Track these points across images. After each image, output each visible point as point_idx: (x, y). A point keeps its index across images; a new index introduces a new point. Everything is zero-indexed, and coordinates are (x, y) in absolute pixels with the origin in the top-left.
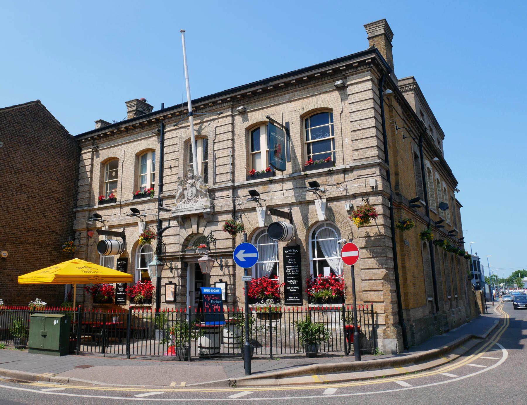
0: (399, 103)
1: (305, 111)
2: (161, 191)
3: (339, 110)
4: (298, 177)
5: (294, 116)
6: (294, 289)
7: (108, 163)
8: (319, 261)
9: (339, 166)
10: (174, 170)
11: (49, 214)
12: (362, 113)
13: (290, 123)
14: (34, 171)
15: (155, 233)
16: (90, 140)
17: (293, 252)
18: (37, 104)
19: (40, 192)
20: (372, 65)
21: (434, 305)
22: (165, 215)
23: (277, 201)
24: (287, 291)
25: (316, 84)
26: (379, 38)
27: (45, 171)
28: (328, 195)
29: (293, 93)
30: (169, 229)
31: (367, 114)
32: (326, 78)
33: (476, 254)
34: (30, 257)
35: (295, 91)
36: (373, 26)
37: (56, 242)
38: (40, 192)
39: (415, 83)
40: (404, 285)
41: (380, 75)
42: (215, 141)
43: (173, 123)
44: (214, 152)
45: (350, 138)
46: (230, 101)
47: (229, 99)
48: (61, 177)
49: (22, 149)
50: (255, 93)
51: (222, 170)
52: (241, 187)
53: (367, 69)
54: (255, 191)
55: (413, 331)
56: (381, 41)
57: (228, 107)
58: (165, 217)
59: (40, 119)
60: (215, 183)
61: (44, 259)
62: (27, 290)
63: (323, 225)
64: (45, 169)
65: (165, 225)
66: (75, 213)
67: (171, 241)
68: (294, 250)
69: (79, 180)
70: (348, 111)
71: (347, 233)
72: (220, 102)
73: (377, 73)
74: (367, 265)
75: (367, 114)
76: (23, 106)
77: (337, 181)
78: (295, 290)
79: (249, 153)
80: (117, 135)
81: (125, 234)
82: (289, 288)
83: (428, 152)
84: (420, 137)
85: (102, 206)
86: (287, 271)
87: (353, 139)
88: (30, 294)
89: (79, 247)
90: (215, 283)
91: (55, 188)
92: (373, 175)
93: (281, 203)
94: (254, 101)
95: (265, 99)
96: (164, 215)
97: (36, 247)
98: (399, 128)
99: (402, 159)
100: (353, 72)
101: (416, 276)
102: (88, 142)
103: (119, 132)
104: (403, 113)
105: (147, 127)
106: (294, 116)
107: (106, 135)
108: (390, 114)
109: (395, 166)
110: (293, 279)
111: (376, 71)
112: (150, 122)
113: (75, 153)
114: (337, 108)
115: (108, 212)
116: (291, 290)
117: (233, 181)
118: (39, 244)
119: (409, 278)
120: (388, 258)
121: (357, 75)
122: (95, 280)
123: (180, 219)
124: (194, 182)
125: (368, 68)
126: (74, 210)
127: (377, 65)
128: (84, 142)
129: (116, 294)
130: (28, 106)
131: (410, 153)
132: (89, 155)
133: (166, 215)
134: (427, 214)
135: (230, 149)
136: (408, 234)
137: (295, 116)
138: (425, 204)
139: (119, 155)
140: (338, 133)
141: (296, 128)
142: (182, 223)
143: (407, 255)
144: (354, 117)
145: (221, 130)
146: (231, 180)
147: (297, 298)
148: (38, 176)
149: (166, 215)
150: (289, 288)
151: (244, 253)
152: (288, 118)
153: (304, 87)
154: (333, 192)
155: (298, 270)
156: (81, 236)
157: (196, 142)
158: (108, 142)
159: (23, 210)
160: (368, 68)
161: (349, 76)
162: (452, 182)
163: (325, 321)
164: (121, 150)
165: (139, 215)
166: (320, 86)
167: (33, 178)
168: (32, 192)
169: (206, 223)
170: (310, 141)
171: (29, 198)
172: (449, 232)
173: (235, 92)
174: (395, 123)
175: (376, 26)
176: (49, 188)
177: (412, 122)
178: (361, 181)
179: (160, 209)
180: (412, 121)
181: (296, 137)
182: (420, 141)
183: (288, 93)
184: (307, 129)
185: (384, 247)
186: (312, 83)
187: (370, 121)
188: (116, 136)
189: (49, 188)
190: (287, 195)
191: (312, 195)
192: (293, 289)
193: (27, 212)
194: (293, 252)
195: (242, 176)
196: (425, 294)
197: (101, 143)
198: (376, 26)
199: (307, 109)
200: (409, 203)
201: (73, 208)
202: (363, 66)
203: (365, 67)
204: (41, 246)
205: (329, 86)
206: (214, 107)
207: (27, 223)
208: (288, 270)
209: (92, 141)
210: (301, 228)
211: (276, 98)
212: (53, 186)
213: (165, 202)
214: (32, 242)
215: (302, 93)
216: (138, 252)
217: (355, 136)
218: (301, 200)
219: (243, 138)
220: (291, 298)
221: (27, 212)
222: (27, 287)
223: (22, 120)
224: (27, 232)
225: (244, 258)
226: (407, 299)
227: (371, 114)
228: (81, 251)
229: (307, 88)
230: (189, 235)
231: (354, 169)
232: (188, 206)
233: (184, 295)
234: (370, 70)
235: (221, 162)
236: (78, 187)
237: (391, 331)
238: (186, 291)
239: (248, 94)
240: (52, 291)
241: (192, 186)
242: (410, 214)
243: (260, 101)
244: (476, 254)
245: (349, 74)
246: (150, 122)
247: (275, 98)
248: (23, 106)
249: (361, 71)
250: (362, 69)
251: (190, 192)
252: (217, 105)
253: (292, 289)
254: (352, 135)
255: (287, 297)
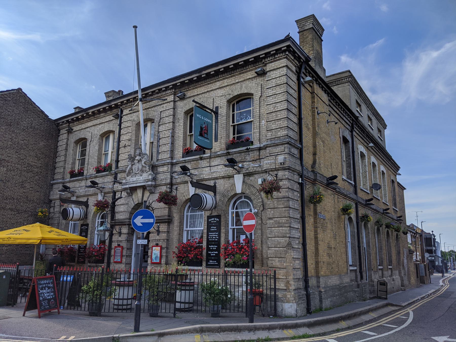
0: (325, 91)
1: (231, 96)
2: (117, 167)
3: (258, 95)
4: (222, 155)
5: (222, 101)
6: (214, 253)
7: (81, 143)
8: (236, 228)
9: (256, 145)
10: (128, 149)
11: (27, 185)
12: (276, 97)
13: (219, 108)
14: (13, 148)
15: (111, 203)
16: (66, 123)
17: (215, 220)
18: (19, 92)
19: (19, 167)
20: (287, 53)
21: (358, 273)
22: (117, 187)
23: (204, 176)
24: (208, 255)
25: (241, 72)
26: (307, 31)
27: (24, 149)
28: (245, 171)
29: (223, 81)
30: (121, 199)
31: (281, 98)
32: (250, 67)
33: (432, 232)
34: (6, 222)
35: (224, 79)
36: (303, 21)
37: (33, 210)
38: (19, 167)
39: (351, 76)
40: (316, 254)
41: (297, 63)
42: (160, 124)
43: (129, 108)
44: (158, 133)
45: (265, 120)
46: (172, 88)
47: (171, 86)
48: (40, 154)
49: (2, 129)
50: (191, 81)
51: (164, 149)
52: (176, 163)
53: (283, 57)
54: (185, 166)
55: (322, 296)
56: (310, 34)
57: (171, 93)
58: (118, 189)
59: (21, 104)
60: (158, 160)
61: (21, 223)
62: (2, 250)
63: (241, 198)
64: (25, 147)
65: (118, 195)
66: (52, 185)
67: (122, 209)
68: (216, 219)
69: (56, 157)
70: (265, 96)
71: (258, 205)
72: (164, 89)
73: (294, 61)
74: (274, 234)
75: (281, 98)
76: (5, 93)
77: (253, 159)
78: (215, 255)
79: (186, 135)
80: (87, 119)
81: (89, 203)
82: (210, 252)
83: (363, 138)
84: (352, 124)
85: (72, 179)
86: (209, 237)
87: (268, 121)
88: (6, 253)
89: (53, 214)
90: (153, 246)
91: (34, 164)
92: (282, 153)
93: (208, 177)
94: (192, 88)
95: (201, 86)
96: (118, 187)
97: (13, 213)
98: (320, 113)
99: (323, 142)
100: (271, 60)
101: (333, 246)
102: (65, 125)
103: (88, 116)
104: (329, 100)
105: (109, 112)
106: (222, 101)
107: (78, 119)
108: (312, 100)
109: (314, 147)
110: (213, 245)
111: (293, 58)
112: (110, 107)
113: (54, 134)
114: (257, 93)
115: (77, 184)
116: (212, 255)
117: (172, 158)
118: (16, 211)
119: (322, 247)
120: (291, 229)
121: (275, 63)
122: (8, 241)
123: (129, 191)
124: (141, 159)
125: (284, 55)
126: (51, 182)
127: (294, 53)
128: (62, 125)
129: (78, 254)
130: (10, 93)
131: (338, 137)
132: (65, 136)
133: (119, 187)
134: (356, 193)
135: (171, 131)
136: (325, 209)
137: (223, 101)
138: (354, 183)
139: (88, 136)
140: (257, 116)
141: (223, 112)
142: (131, 194)
143: (320, 227)
144: (270, 101)
145: (164, 114)
146: (170, 157)
147: (215, 262)
148: (18, 152)
149: (119, 187)
150: (210, 252)
151: (141, 218)
152: (218, 103)
153: (232, 75)
154: (249, 168)
155: (218, 236)
156: (56, 205)
157: (145, 126)
158: (80, 125)
159: (2, 181)
160: (284, 55)
161: (268, 63)
162: (395, 168)
163: (237, 284)
164: (89, 132)
165: (98, 187)
166: (245, 74)
167: (13, 154)
168: (11, 166)
169: (149, 194)
170: (236, 123)
171: (8, 171)
172: (384, 210)
173: (175, 81)
174: (317, 108)
175: (305, 21)
176: (28, 164)
177: (341, 110)
178: (272, 158)
179: (115, 182)
180: (341, 108)
181: (223, 120)
182: (352, 127)
183: (218, 81)
184: (233, 113)
185: (289, 218)
186: (238, 71)
187: (283, 104)
188: (85, 120)
189: (28, 164)
190: (213, 171)
191: (232, 171)
192: (213, 254)
193: (5, 183)
194: (215, 220)
195: (179, 154)
196: (346, 264)
197: (75, 126)
198: (305, 21)
199: (232, 95)
200: (327, 180)
201: (51, 181)
202: (280, 53)
203: (281, 55)
204: (18, 212)
205: (252, 74)
206: (160, 94)
207: (5, 192)
208: (210, 237)
209: (68, 124)
210: (222, 200)
211: (210, 85)
212: (32, 162)
213: (119, 176)
214: (10, 208)
215: (230, 81)
216: (98, 219)
217: (270, 118)
218: (223, 175)
219: (182, 121)
220: (211, 261)
221: (5, 183)
222: (3, 246)
223: (3, 104)
224: (5, 200)
225: (141, 223)
226: (318, 267)
227: (285, 97)
228: (54, 217)
229: (234, 76)
230: (136, 205)
231: (267, 147)
232: (134, 179)
233: (130, 256)
234: (286, 58)
235: (163, 142)
236: (56, 163)
237: (292, 296)
238: (132, 254)
239: (186, 82)
240: (28, 251)
241: (139, 161)
242: (329, 190)
243: (196, 88)
244: (432, 232)
245: (268, 62)
246: (110, 107)
247: (208, 86)
248: (5, 93)
249: (278, 58)
250: (279, 57)
251: (137, 168)
252: (162, 92)
253: (212, 254)
254: (267, 117)
255: (207, 261)
